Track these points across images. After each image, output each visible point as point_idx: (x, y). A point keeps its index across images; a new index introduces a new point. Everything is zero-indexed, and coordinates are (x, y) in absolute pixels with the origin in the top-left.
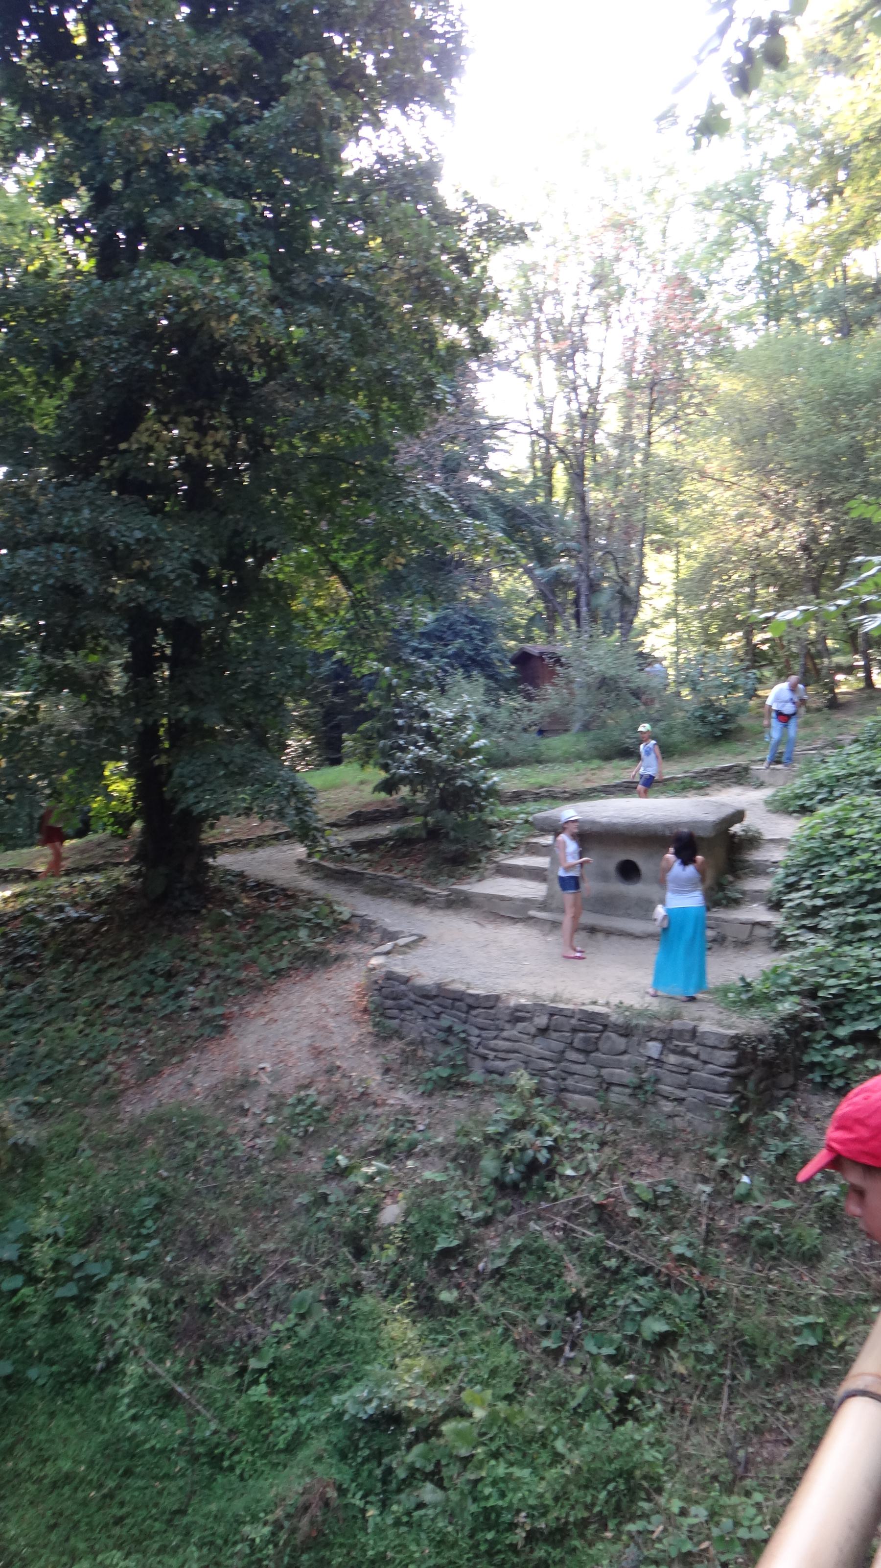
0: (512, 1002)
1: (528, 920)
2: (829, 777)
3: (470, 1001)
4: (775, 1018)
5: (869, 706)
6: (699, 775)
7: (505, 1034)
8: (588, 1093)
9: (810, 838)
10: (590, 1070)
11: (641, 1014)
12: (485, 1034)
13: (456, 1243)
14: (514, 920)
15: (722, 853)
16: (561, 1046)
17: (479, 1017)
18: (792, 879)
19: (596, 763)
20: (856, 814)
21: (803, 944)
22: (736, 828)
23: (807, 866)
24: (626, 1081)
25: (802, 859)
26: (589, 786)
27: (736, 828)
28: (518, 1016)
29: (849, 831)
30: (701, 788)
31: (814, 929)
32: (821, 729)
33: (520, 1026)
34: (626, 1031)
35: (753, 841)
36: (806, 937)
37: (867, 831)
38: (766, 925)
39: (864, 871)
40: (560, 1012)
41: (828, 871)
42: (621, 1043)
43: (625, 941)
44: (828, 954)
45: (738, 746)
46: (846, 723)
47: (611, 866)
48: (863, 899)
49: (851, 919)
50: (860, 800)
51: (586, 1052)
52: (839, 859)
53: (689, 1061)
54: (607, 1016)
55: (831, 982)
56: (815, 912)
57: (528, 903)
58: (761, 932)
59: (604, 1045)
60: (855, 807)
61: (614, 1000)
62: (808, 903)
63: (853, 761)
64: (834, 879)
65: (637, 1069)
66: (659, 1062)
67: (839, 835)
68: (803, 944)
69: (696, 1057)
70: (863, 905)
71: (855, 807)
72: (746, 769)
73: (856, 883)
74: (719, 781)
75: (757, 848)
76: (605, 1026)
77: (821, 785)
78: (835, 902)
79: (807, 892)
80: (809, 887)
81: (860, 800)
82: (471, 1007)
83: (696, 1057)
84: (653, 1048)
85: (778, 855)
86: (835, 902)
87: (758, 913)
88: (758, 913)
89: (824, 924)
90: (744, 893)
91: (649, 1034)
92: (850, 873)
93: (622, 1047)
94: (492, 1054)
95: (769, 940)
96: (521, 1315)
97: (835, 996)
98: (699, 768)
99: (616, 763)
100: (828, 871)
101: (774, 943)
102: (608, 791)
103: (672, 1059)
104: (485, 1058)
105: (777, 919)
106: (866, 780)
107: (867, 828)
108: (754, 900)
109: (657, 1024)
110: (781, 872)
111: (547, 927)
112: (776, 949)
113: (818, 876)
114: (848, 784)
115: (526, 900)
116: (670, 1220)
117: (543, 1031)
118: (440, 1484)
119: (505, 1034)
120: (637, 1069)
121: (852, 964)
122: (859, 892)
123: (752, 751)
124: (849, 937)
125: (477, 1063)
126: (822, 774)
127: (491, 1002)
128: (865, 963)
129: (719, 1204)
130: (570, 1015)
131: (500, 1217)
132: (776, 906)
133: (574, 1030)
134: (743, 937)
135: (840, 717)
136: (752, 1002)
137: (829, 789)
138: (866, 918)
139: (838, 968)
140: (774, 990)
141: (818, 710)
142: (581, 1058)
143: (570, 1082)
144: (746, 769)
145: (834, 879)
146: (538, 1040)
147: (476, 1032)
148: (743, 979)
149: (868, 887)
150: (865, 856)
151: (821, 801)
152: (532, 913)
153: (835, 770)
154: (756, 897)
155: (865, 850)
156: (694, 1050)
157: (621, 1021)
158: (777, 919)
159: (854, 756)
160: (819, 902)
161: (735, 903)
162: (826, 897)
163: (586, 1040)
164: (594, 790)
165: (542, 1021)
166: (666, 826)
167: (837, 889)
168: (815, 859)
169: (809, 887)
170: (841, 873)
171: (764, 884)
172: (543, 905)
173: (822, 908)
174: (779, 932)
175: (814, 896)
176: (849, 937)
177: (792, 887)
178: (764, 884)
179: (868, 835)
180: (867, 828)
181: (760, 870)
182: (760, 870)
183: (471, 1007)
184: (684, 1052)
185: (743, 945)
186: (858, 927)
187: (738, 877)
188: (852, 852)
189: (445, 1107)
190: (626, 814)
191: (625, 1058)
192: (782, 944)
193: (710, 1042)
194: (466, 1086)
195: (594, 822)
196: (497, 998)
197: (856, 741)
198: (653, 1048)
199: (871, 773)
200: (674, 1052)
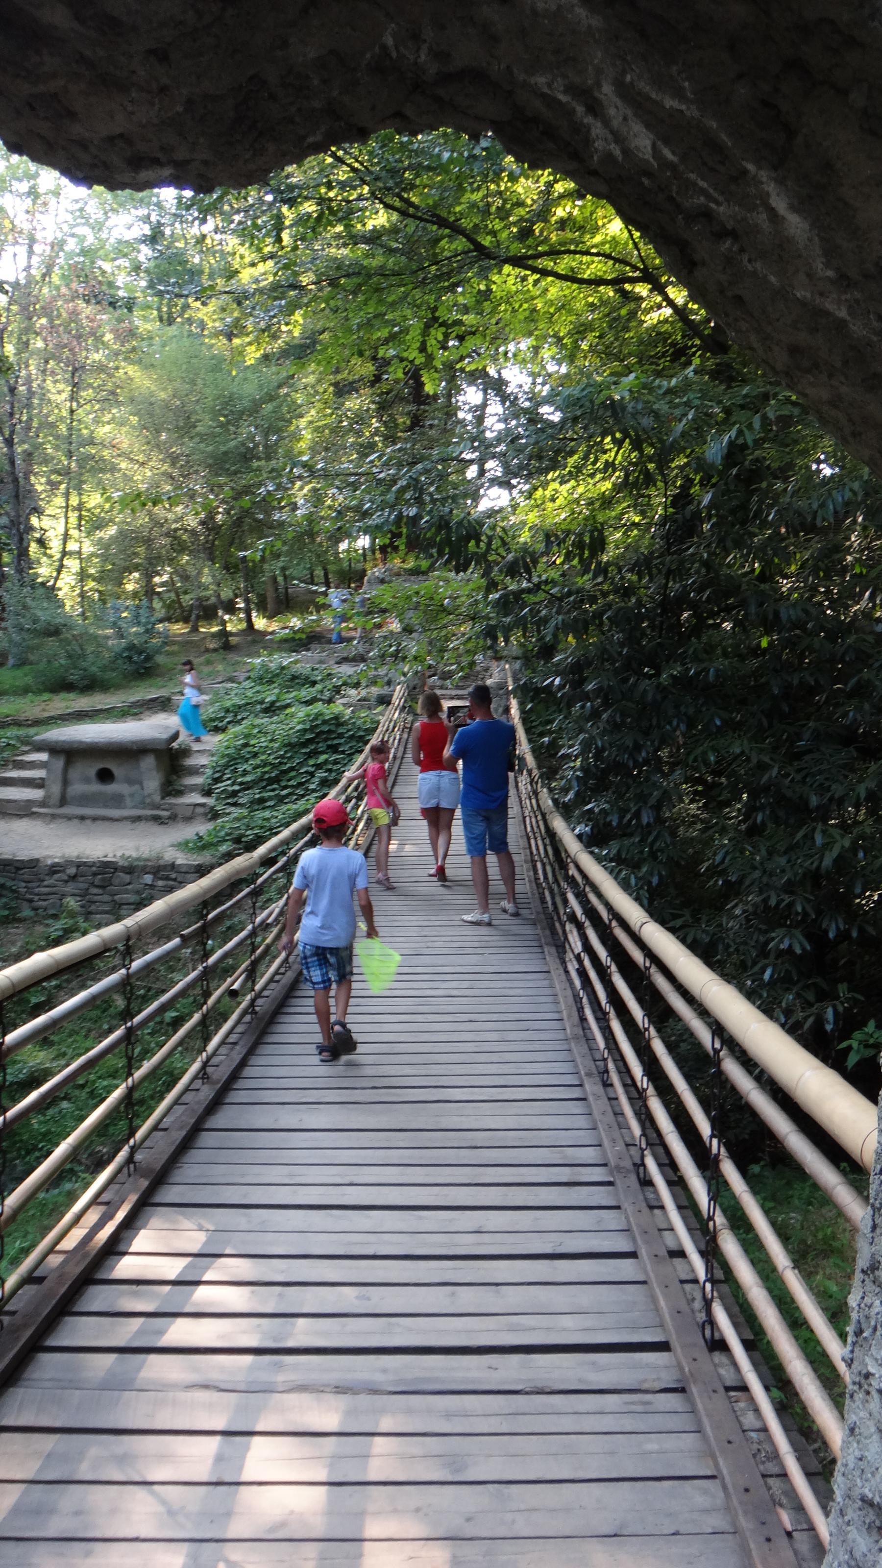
0: (49, 862)
1: (32, 815)
2: (234, 705)
3: (17, 865)
4: (218, 854)
5: (254, 649)
6: (134, 705)
7: (45, 883)
8: (106, 912)
9: (227, 748)
10: (106, 898)
11: (138, 859)
12: (30, 885)
13: (43, 999)
14: (20, 816)
15: (171, 759)
16: (85, 886)
17: (25, 874)
18: (217, 775)
19: (46, 696)
20: (256, 731)
21: (229, 814)
22: (175, 745)
23: (227, 766)
24: (131, 901)
25: (223, 761)
26: (46, 714)
27: (175, 745)
28: (55, 869)
29: (252, 742)
30: (136, 714)
31: (235, 805)
32: (220, 667)
33: (56, 876)
34: (130, 870)
35: (185, 752)
36: (232, 809)
37: (263, 741)
38: (203, 805)
39: (264, 766)
40: (85, 864)
41: (241, 768)
42: (127, 878)
43: (106, 823)
44: (245, 817)
45: (159, 681)
46: (238, 663)
47: (92, 772)
48: (264, 784)
49: (257, 796)
50: (258, 721)
51: (103, 887)
52: (247, 760)
53: (171, 883)
54: (117, 863)
55: (249, 832)
56: (234, 794)
57: (30, 803)
58: (200, 810)
59: (116, 881)
60: (254, 726)
61: (119, 854)
62: (230, 789)
63: (249, 693)
64: (245, 773)
65: (138, 892)
66: (152, 886)
67: (246, 745)
68: (229, 814)
69: (175, 880)
70: (264, 787)
71: (254, 726)
72: (169, 700)
73: (259, 774)
74: (149, 709)
75: (188, 757)
76: (116, 869)
77: (227, 711)
78: (246, 786)
79: (229, 782)
80: (229, 779)
81: (258, 721)
82: (18, 869)
83: (175, 880)
84: (148, 879)
85: (203, 760)
86: (246, 786)
87: (196, 798)
88: (196, 798)
89: (241, 801)
90: (186, 786)
91: (145, 870)
92: (254, 768)
93: (128, 881)
94: (36, 898)
95: (206, 814)
96: (93, 1026)
97: (252, 840)
98: (133, 699)
99: (63, 695)
100: (241, 768)
101: (209, 816)
102: (81, 716)
103: (160, 883)
104: (31, 901)
105: (210, 801)
106: (258, 707)
107: (263, 739)
108: (192, 791)
109: (150, 864)
110: (209, 772)
111: (48, 819)
112: (210, 820)
113: (235, 771)
114: (246, 710)
115: (28, 801)
116: (170, 967)
117: (73, 878)
118: (69, 1100)
119: (45, 883)
120: (138, 892)
121: (260, 822)
122: (261, 779)
123: (171, 684)
124: (256, 807)
125: (25, 904)
126: (228, 704)
127: (33, 863)
128: (267, 820)
129: (196, 957)
130: (93, 864)
131: (64, 985)
132: (208, 793)
133: (95, 874)
134: (188, 814)
135: (233, 657)
136: (204, 847)
137: (235, 714)
138: (266, 795)
139: (252, 825)
140: (215, 840)
141: (215, 650)
142: (100, 891)
143: (93, 908)
144: (169, 700)
145: (245, 773)
146: (70, 884)
147: (24, 884)
148: (197, 834)
149: (267, 776)
150: (263, 757)
151: (229, 722)
152: (35, 810)
153: (237, 701)
154: (193, 788)
155: (264, 753)
156: (173, 876)
157: (126, 864)
158: (210, 801)
159: (249, 690)
160: (237, 788)
161: (180, 793)
162: (241, 784)
163: (103, 880)
164: (51, 718)
165: (72, 871)
166: (133, 742)
167: (248, 778)
168: (231, 761)
169: (229, 779)
170: (249, 769)
171: (198, 780)
172: (43, 804)
173: (239, 791)
174: (212, 808)
175: (233, 784)
176: (256, 807)
177: (217, 780)
178: (198, 780)
179: (264, 744)
180: (263, 739)
181: (195, 771)
182: (195, 771)
183: (18, 869)
184: (167, 878)
185: (189, 819)
186: (262, 801)
187: (179, 777)
188: (255, 755)
189: (9, 934)
190: (103, 735)
191: (129, 887)
192: (214, 815)
193: (184, 870)
194: (20, 920)
195: (81, 742)
196: (37, 860)
197: (249, 678)
198: (148, 879)
199: (262, 702)
200: (161, 879)
